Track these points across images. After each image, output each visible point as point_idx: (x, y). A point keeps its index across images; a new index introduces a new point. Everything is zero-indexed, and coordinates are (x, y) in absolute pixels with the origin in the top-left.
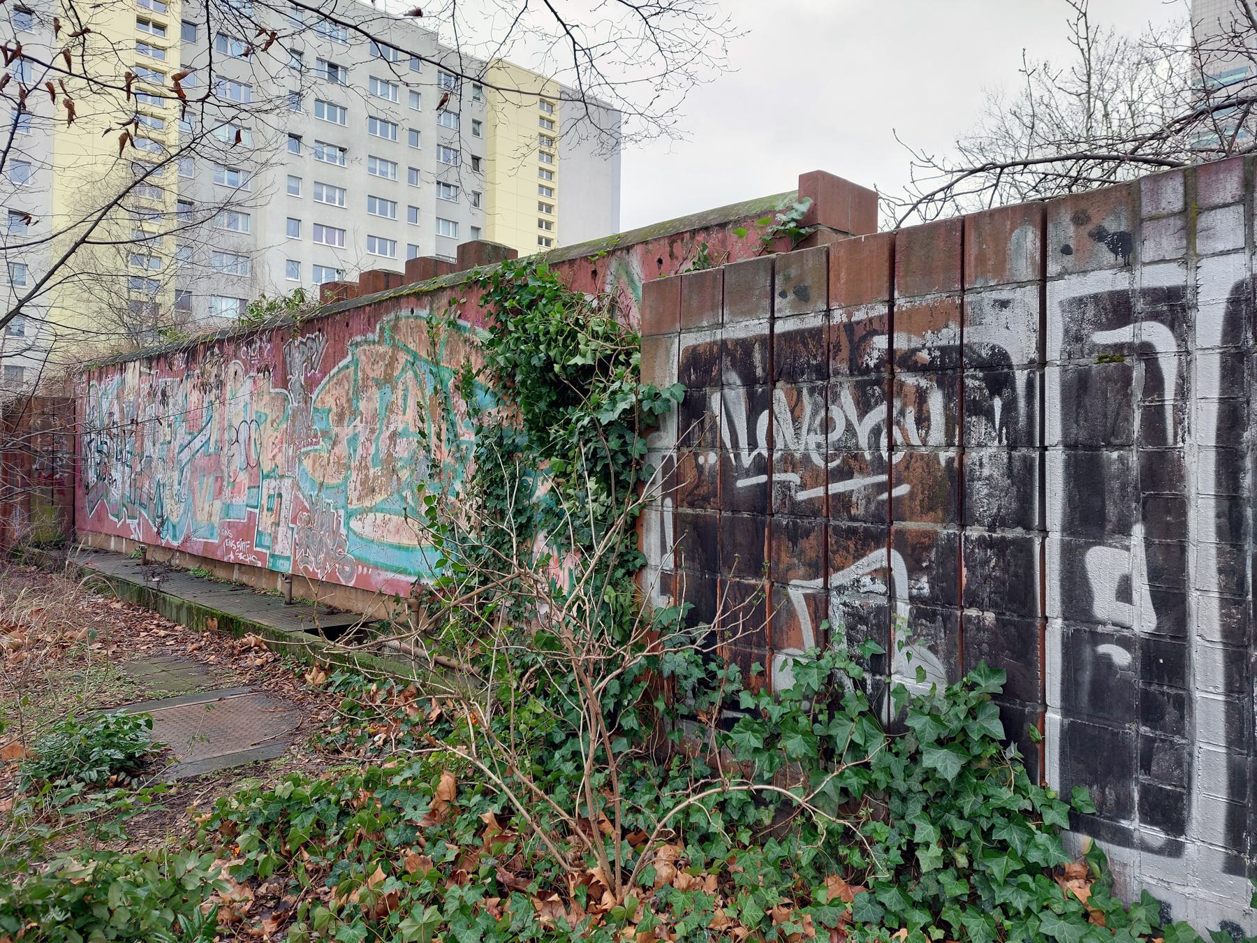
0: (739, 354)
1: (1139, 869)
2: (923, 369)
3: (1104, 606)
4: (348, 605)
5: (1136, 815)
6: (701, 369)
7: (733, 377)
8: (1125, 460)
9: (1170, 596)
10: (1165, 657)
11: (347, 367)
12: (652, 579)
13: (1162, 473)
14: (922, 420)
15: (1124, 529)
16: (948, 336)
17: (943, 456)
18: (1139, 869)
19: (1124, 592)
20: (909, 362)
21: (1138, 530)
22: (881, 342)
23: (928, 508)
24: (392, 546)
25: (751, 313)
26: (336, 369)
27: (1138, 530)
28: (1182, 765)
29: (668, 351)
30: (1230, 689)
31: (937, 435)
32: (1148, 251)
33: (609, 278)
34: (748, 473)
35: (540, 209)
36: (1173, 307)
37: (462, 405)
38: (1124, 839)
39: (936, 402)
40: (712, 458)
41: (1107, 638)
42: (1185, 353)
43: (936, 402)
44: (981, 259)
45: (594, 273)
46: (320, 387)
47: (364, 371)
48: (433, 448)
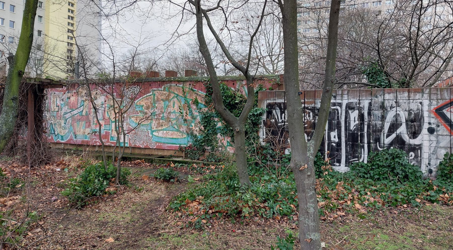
0: (279, 105)
1: (336, 168)
2: (309, 109)
3: (332, 139)
4: (152, 153)
5: (398, 131)
6: (271, 107)
7: (278, 108)
8: (335, 122)
9: (340, 138)
10: (339, 144)
11: (150, 95)
12: (261, 140)
13: (339, 123)
14: (309, 116)
15: (335, 130)
16: (313, 105)
17: (312, 121)
18: (336, 168)
19: (335, 137)
20: (307, 108)
21: (336, 130)
22: (303, 105)
23: (310, 128)
24: (170, 138)
25: (281, 99)
26: (146, 96)
27: (336, 130)
28: (341, 156)
29: (264, 103)
30: (346, 147)
31: (311, 118)
32: (337, 98)
33: (237, 85)
34: (280, 123)
35: (69, 11)
36: (340, 105)
37: (194, 107)
38: (334, 165)
39: (311, 114)
40: (273, 120)
41: (333, 143)
42: (341, 110)
43: (311, 114)
44: (317, 96)
45: (234, 84)
46: (138, 100)
47: (157, 97)
48: (184, 116)
